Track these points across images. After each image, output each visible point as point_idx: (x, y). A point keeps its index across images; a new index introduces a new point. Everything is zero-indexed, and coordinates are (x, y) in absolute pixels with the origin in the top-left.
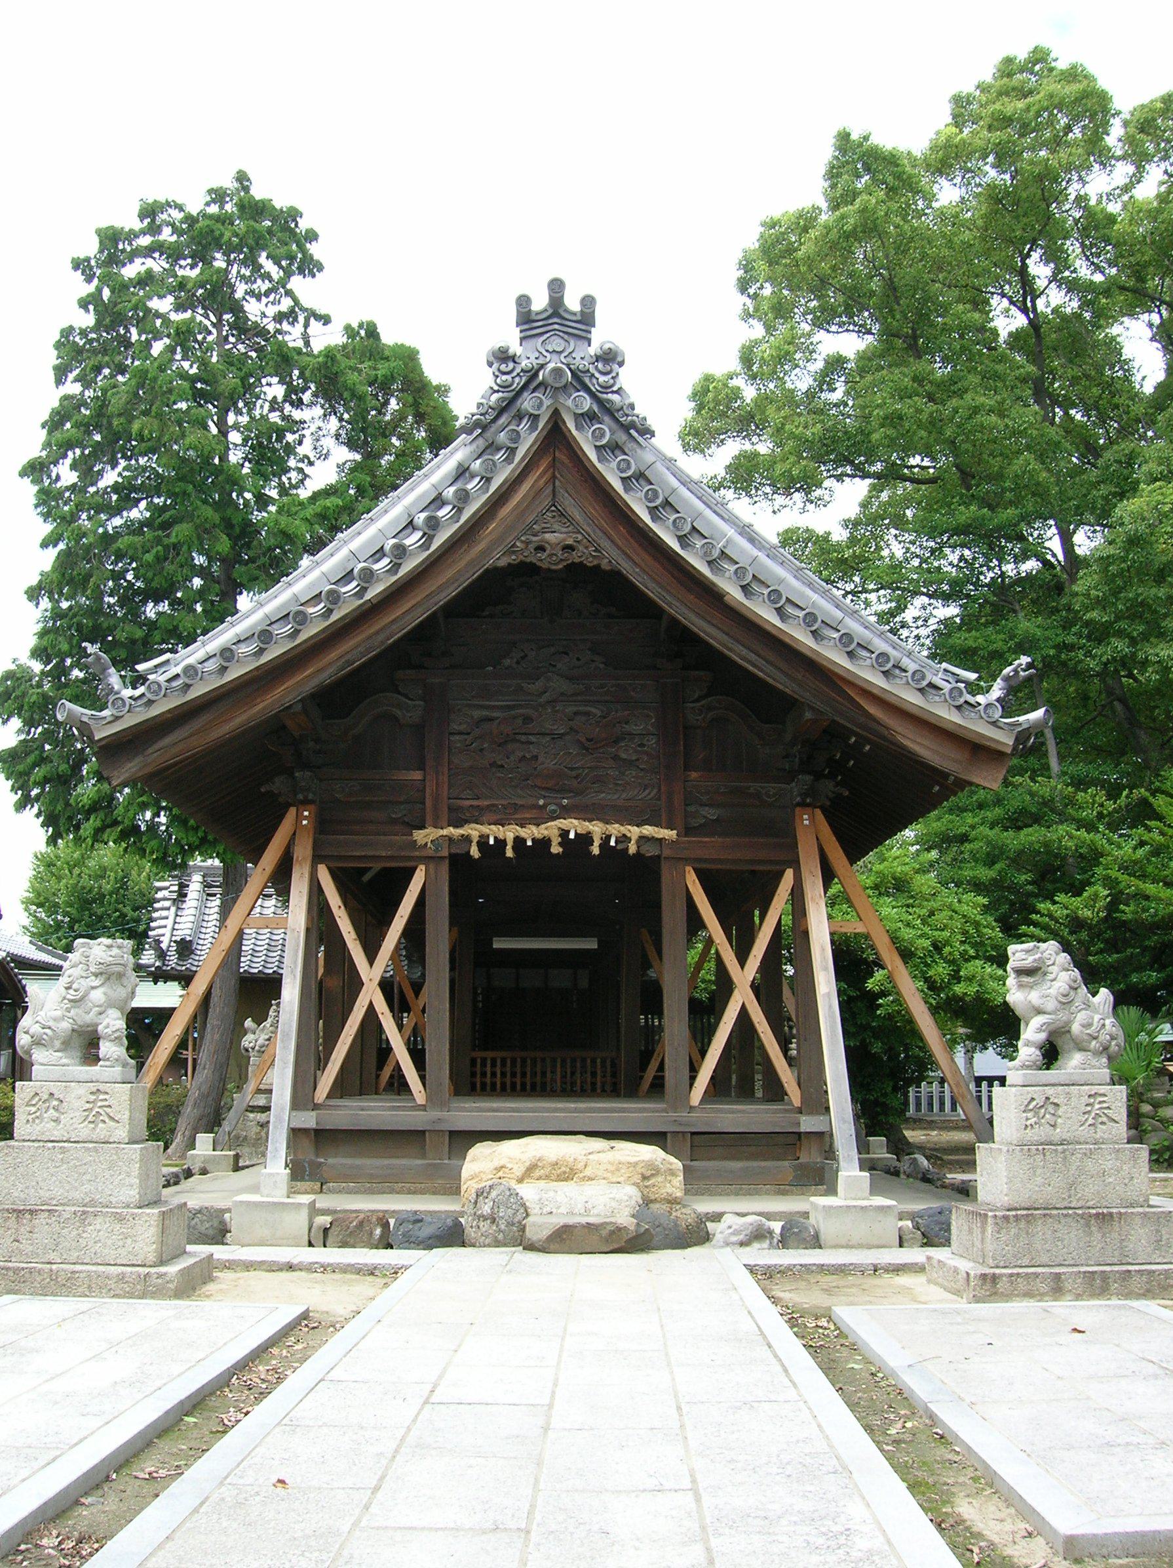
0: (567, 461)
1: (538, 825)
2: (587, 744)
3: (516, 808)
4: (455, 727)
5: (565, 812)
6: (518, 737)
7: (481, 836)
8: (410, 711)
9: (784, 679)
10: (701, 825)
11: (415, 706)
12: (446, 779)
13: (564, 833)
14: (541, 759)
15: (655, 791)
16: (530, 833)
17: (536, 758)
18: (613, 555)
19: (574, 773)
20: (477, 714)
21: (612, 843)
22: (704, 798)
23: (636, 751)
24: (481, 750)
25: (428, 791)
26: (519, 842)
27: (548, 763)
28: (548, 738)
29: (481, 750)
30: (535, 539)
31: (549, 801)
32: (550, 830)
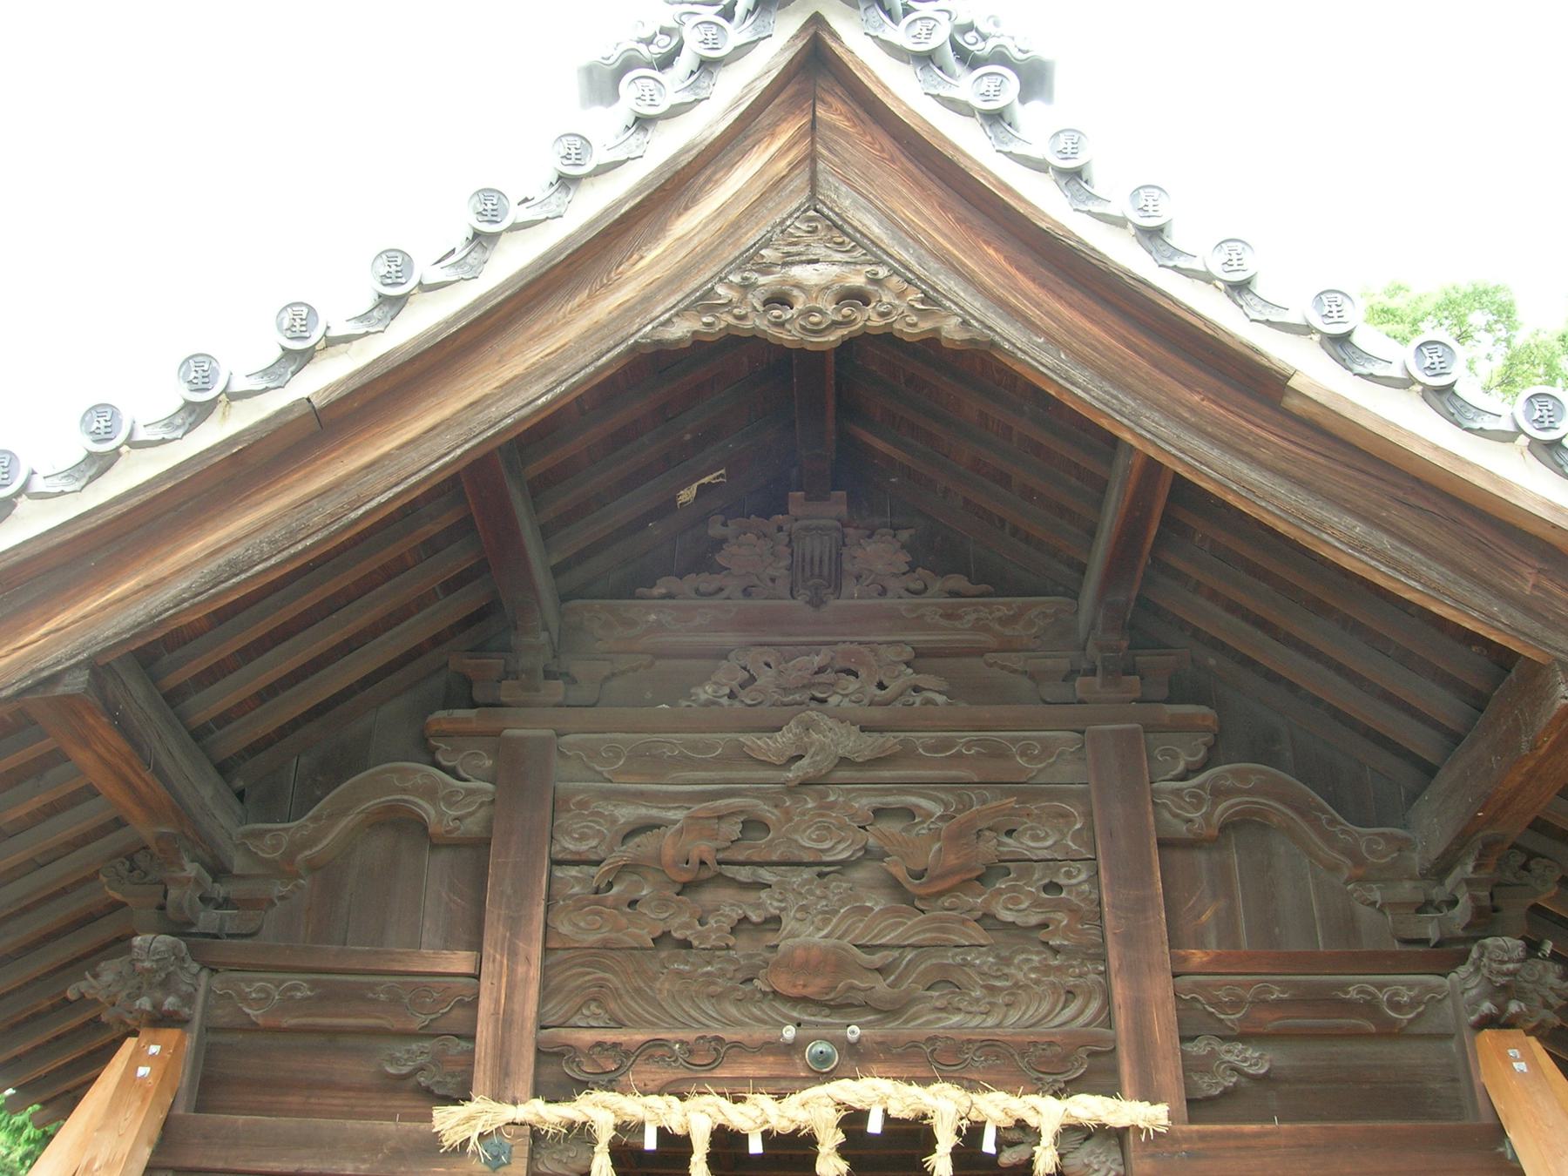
0: (843, 124)
1: (780, 1096)
2: (911, 885)
3: (721, 1051)
4: (569, 845)
5: (857, 1059)
6: (730, 871)
7: (622, 1128)
8: (453, 799)
9: (1480, 598)
10: (1226, 1093)
11: (470, 792)
12: (535, 973)
13: (853, 1120)
14: (789, 924)
15: (1095, 1006)
16: (758, 1117)
17: (774, 922)
18: (972, 300)
19: (877, 959)
20: (627, 813)
21: (989, 1146)
22: (1230, 1018)
23: (1037, 904)
24: (633, 903)
25: (485, 1005)
26: (726, 1141)
27: (805, 934)
28: (807, 874)
29: (633, 903)
30: (762, 280)
31: (812, 1032)
32: (814, 1110)
